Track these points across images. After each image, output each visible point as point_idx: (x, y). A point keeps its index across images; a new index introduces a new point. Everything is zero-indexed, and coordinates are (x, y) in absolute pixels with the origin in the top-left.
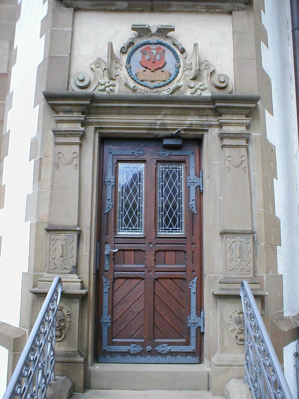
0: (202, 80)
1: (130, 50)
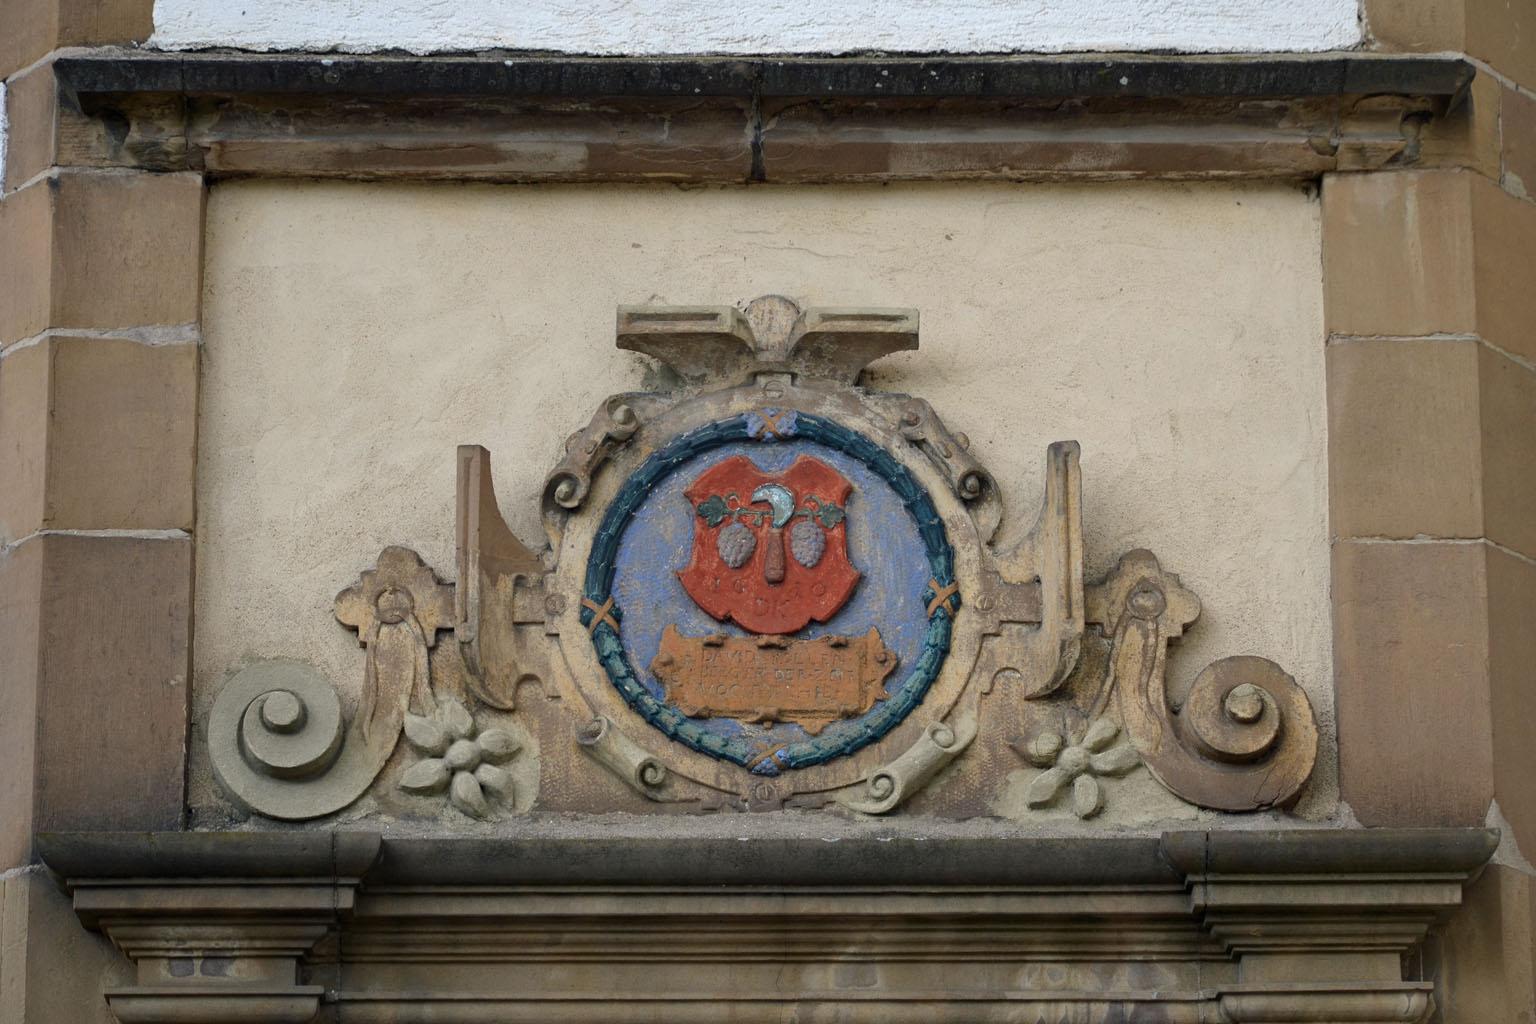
0: (1109, 699)
1: (611, 485)
